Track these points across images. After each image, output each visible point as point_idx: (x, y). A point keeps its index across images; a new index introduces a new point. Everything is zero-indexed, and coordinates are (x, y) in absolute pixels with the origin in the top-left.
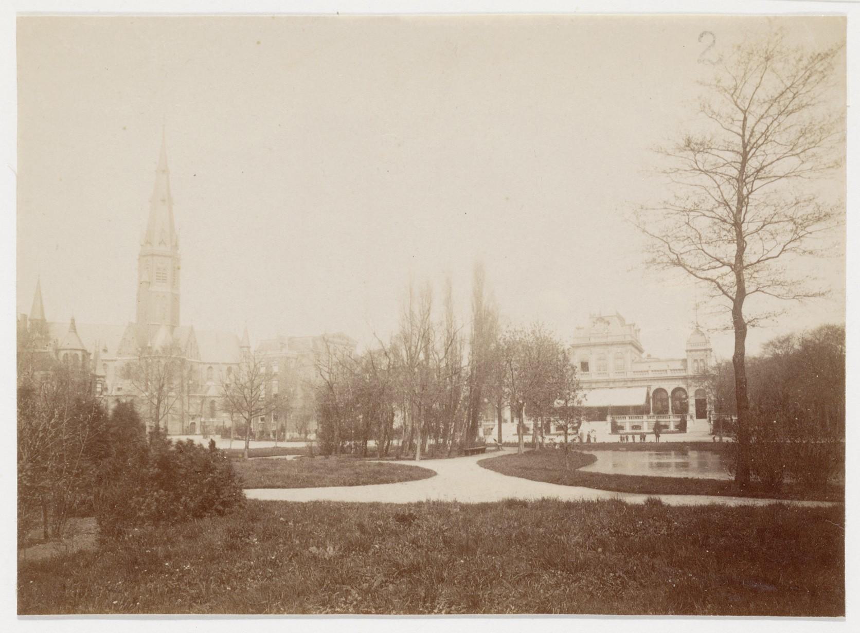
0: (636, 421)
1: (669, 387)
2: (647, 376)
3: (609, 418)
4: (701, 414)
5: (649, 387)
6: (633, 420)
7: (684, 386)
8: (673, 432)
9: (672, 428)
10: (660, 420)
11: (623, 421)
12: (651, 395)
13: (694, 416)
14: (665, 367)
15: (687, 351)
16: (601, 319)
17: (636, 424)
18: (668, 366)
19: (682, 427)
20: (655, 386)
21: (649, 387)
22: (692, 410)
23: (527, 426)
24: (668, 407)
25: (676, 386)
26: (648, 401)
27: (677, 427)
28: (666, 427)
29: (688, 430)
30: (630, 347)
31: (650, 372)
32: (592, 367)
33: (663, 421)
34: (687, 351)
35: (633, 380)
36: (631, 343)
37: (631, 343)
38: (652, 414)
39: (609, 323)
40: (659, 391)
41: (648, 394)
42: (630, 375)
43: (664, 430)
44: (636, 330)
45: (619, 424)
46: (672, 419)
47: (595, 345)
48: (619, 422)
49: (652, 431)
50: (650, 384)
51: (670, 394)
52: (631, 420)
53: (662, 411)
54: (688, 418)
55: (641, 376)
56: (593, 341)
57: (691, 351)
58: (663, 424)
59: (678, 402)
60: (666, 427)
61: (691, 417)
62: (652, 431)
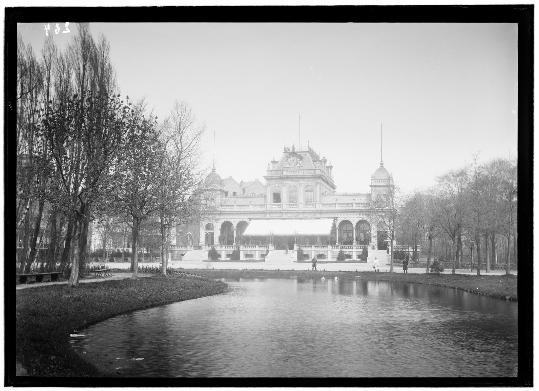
0: (321, 251)
3: (296, 247)
4: (382, 246)
5: (335, 219)
6: (318, 249)
7: (368, 219)
8: (354, 262)
9: (355, 257)
10: (344, 250)
11: (308, 249)
12: (337, 226)
13: (376, 247)
14: (352, 201)
19: (363, 257)
20: (341, 218)
21: (335, 219)
22: (374, 242)
23: (219, 253)
24: (352, 238)
25: (240, 220)
26: (333, 231)
27: (359, 256)
29: (368, 261)
30: (319, 181)
31: (337, 205)
32: (284, 198)
33: (346, 251)
34: (371, 186)
36: (321, 177)
37: (321, 177)
38: (337, 244)
39: (301, 158)
40: (346, 223)
41: (334, 225)
42: (319, 207)
43: (347, 260)
44: (328, 167)
45: (305, 253)
48: (305, 251)
49: (336, 260)
50: (336, 216)
51: (354, 226)
52: (316, 249)
53: (348, 242)
54: (369, 249)
56: (285, 173)
57: (375, 186)
59: (362, 235)
60: (349, 256)
61: (373, 248)
62: (336, 260)
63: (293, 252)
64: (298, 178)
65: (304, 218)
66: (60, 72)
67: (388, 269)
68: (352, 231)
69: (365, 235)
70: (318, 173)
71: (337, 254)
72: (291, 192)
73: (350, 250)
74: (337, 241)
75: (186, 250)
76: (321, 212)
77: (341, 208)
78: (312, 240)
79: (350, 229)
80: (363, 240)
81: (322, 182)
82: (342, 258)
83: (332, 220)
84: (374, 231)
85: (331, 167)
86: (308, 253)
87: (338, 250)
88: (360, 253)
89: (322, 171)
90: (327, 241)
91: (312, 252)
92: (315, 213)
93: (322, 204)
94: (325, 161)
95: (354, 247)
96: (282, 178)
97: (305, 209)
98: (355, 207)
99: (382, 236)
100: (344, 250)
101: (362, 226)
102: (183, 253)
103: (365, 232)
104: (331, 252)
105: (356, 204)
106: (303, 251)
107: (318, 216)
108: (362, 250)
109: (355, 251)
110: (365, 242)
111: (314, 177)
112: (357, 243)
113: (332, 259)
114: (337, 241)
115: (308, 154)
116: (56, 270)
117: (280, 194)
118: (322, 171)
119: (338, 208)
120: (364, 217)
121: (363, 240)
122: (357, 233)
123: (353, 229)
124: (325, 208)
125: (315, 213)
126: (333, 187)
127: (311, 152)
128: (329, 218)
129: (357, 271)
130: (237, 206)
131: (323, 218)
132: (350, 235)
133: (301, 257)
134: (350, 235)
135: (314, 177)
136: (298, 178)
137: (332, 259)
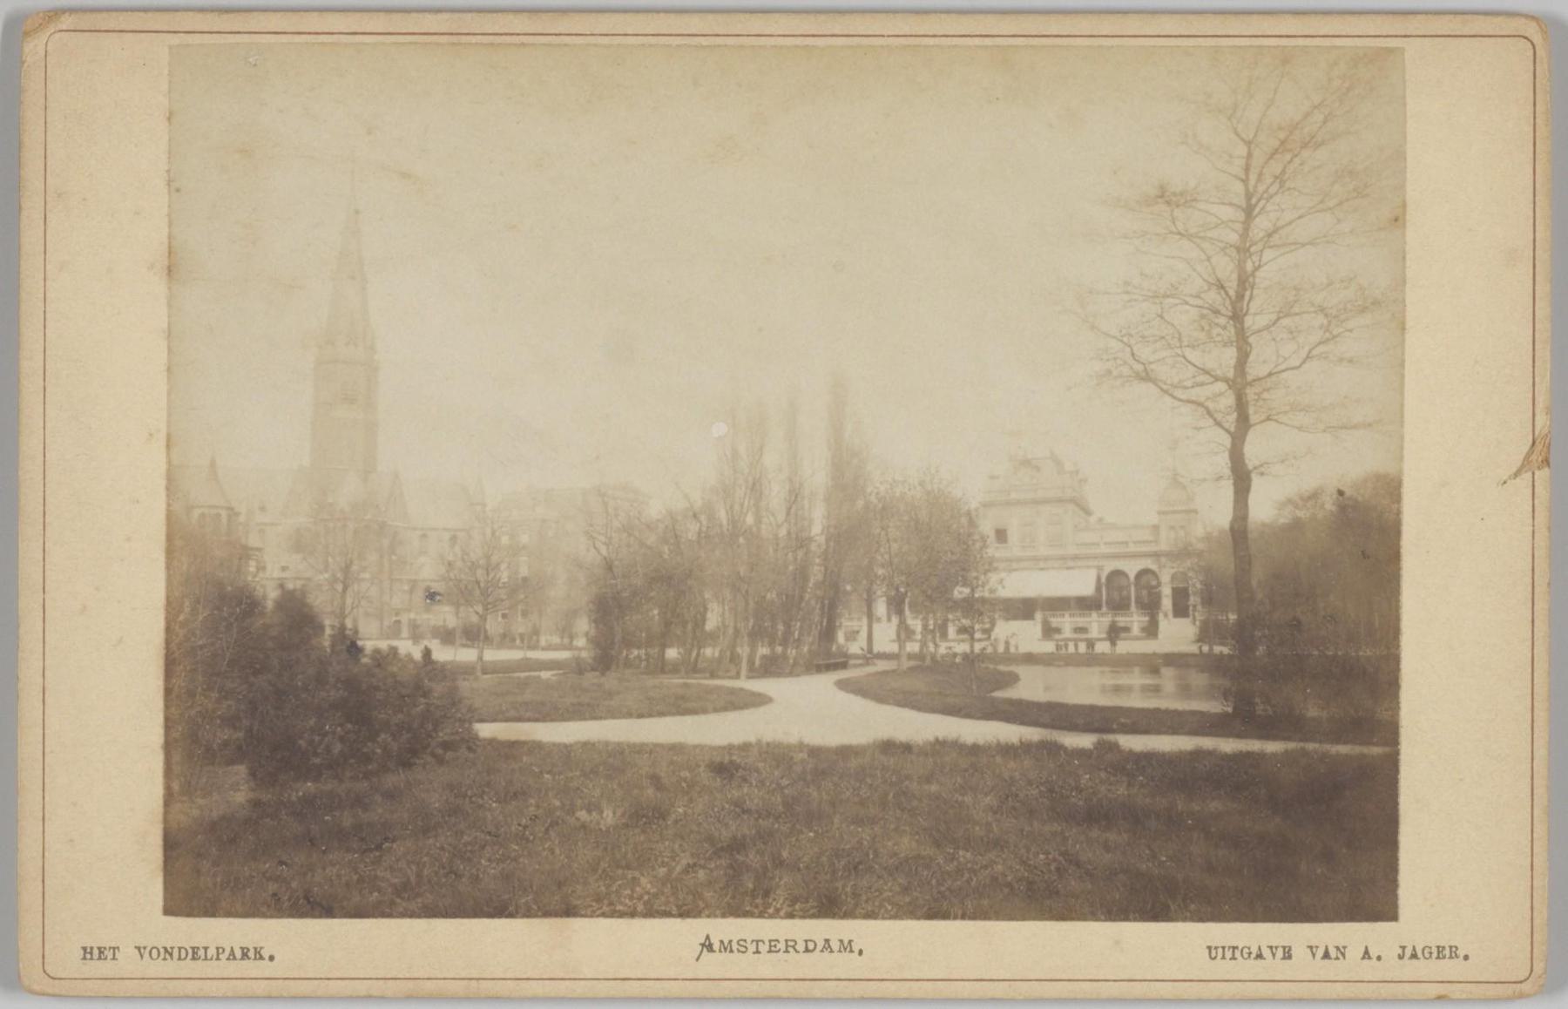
0: (1081, 621)
1: (1132, 568)
2: (1128, 550)
3: (1039, 616)
4: (1181, 610)
5: (1100, 568)
7: (1154, 567)
8: (1137, 638)
9: (1136, 630)
10: (1117, 619)
12: (1103, 580)
15: (1159, 513)
16: (1026, 463)
17: (1080, 625)
19: (1151, 630)
20: (1110, 566)
21: (1100, 568)
22: (1167, 603)
23: (912, 627)
24: (1129, 598)
26: (1098, 589)
27: (1143, 630)
28: (1127, 629)
29: (1160, 636)
32: (1013, 536)
33: (1122, 620)
34: (1159, 513)
35: (1076, 558)
36: (1073, 501)
37: (1073, 501)
38: (1104, 609)
39: (1038, 469)
41: (1099, 579)
42: (1072, 550)
44: (1081, 481)
45: (1054, 625)
46: (1136, 618)
47: (1019, 503)
48: (1055, 621)
50: (1101, 564)
52: (1072, 619)
53: (1120, 606)
55: (1117, 551)
56: (1014, 496)
58: (1122, 625)
59: (1145, 592)
61: (1166, 615)
64: (1036, 502)
65: (1047, 569)
68: (1129, 586)
69: (1150, 594)
73: (1128, 619)
78: (1058, 604)
84: (1166, 591)
87: (1107, 620)
90: (1086, 604)
91: (1066, 622)
93: (1078, 545)
96: (1008, 504)
99: (1180, 597)
100: (1117, 619)
101: (1144, 579)
102: (856, 629)
104: (1097, 624)
105: (1106, 543)
107: (1071, 564)
108: (1147, 619)
110: (1150, 606)
111: (1060, 501)
112: (1137, 607)
114: (1133, 604)
116: (1153, 816)
117: (1005, 530)
119: (1104, 549)
120: (1149, 564)
121: (1146, 601)
122: (1137, 591)
126: (1088, 513)
128: (1088, 567)
130: (1106, 543)
131: (1079, 567)
133: (1049, 631)
135: (1060, 501)
136: (1036, 502)
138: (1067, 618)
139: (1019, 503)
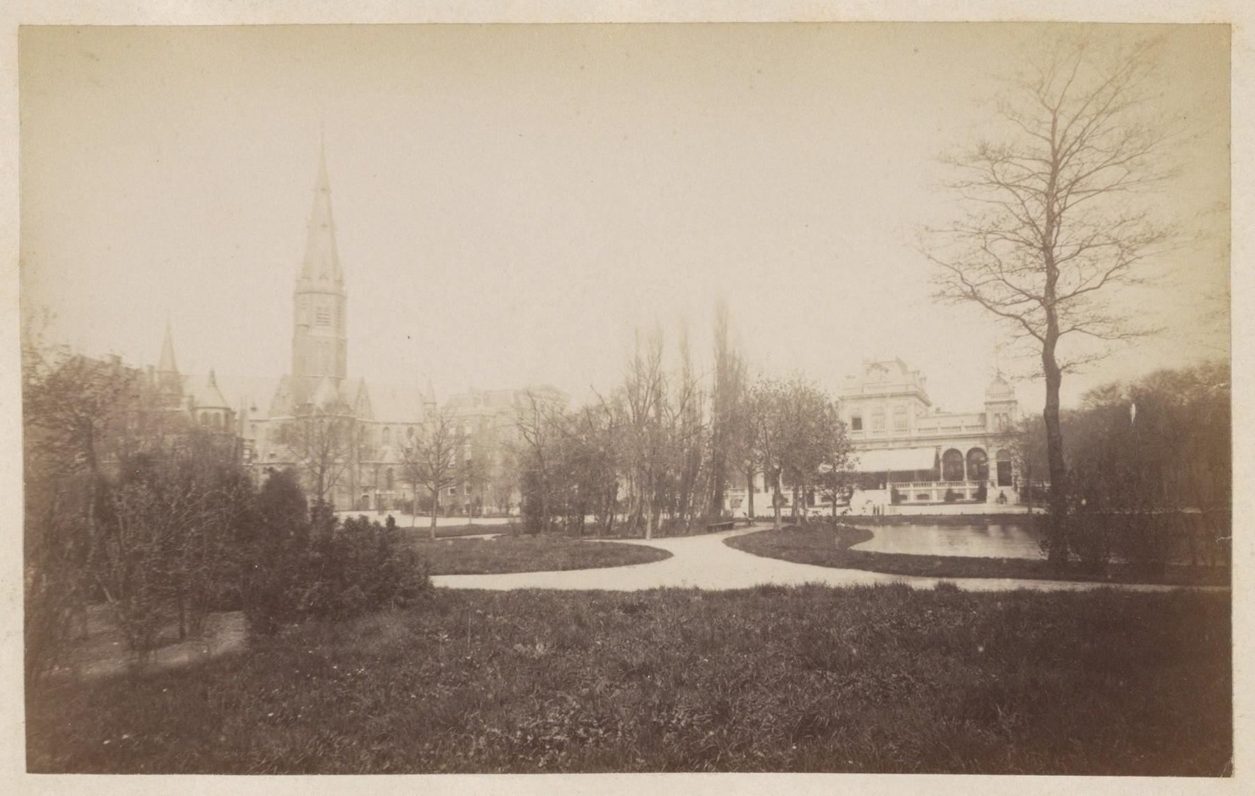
0: (922, 490)
3: (889, 486)
4: (1004, 480)
5: (938, 448)
6: (918, 488)
7: (983, 446)
9: (968, 497)
11: (905, 489)
12: (941, 457)
13: (996, 483)
18: (939, 423)
19: (981, 496)
20: (946, 445)
21: (938, 448)
22: (993, 474)
23: (785, 497)
24: (963, 472)
27: (974, 496)
28: (961, 496)
30: (913, 399)
31: (939, 430)
32: (867, 424)
33: (956, 489)
34: (986, 403)
37: (915, 395)
38: (942, 480)
40: (953, 452)
41: (937, 456)
42: (915, 434)
43: (958, 500)
44: (921, 379)
45: (901, 493)
47: (870, 397)
48: (902, 490)
49: (943, 501)
52: (916, 488)
53: (956, 477)
54: (988, 485)
57: (991, 403)
60: (961, 496)
61: (993, 484)
62: (943, 501)
63: (886, 493)
65: (896, 449)
66: (1117, 184)
67: (1024, 510)
70: (912, 389)
71: (944, 493)
72: (897, 413)
74: (942, 476)
75: (742, 494)
76: (918, 440)
77: (968, 433)
78: (905, 477)
79: (959, 459)
80: (977, 474)
81: (917, 400)
82: (951, 498)
83: (935, 450)
85: (925, 379)
86: (905, 494)
87: (944, 488)
88: (976, 491)
89: (915, 386)
90: (925, 477)
91: (911, 491)
92: (866, 443)
93: (919, 430)
94: (918, 372)
95: (967, 484)
96: (862, 398)
97: (875, 437)
98: (964, 432)
99: (1003, 468)
100: (953, 487)
101: (975, 456)
102: (740, 498)
103: (978, 462)
104: (936, 491)
105: (942, 428)
106: (898, 491)
107: (913, 444)
108: (977, 487)
109: (968, 488)
111: (906, 395)
112: (968, 478)
113: (823, 502)
115: (896, 364)
118: (915, 386)
119: (940, 433)
122: (968, 465)
123: (962, 460)
124: (923, 434)
125: (866, 443)
127: (898, 361)
129: (984, 514)
131: (922, 447)
132: (959, 468)
133: (897, 499)
134: (959, 468)
135: (906, 395)
137: (823, 502)
138: (911, 487)
139: (870, 397)
